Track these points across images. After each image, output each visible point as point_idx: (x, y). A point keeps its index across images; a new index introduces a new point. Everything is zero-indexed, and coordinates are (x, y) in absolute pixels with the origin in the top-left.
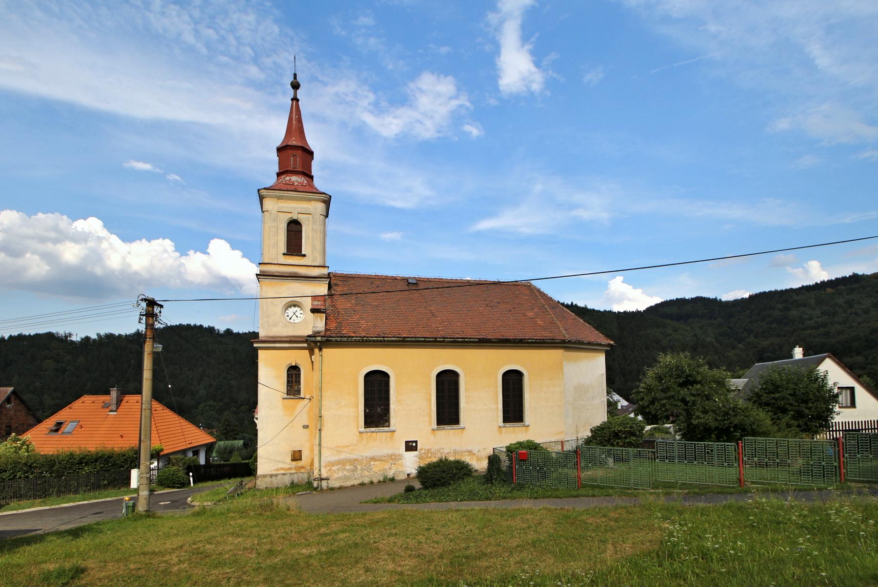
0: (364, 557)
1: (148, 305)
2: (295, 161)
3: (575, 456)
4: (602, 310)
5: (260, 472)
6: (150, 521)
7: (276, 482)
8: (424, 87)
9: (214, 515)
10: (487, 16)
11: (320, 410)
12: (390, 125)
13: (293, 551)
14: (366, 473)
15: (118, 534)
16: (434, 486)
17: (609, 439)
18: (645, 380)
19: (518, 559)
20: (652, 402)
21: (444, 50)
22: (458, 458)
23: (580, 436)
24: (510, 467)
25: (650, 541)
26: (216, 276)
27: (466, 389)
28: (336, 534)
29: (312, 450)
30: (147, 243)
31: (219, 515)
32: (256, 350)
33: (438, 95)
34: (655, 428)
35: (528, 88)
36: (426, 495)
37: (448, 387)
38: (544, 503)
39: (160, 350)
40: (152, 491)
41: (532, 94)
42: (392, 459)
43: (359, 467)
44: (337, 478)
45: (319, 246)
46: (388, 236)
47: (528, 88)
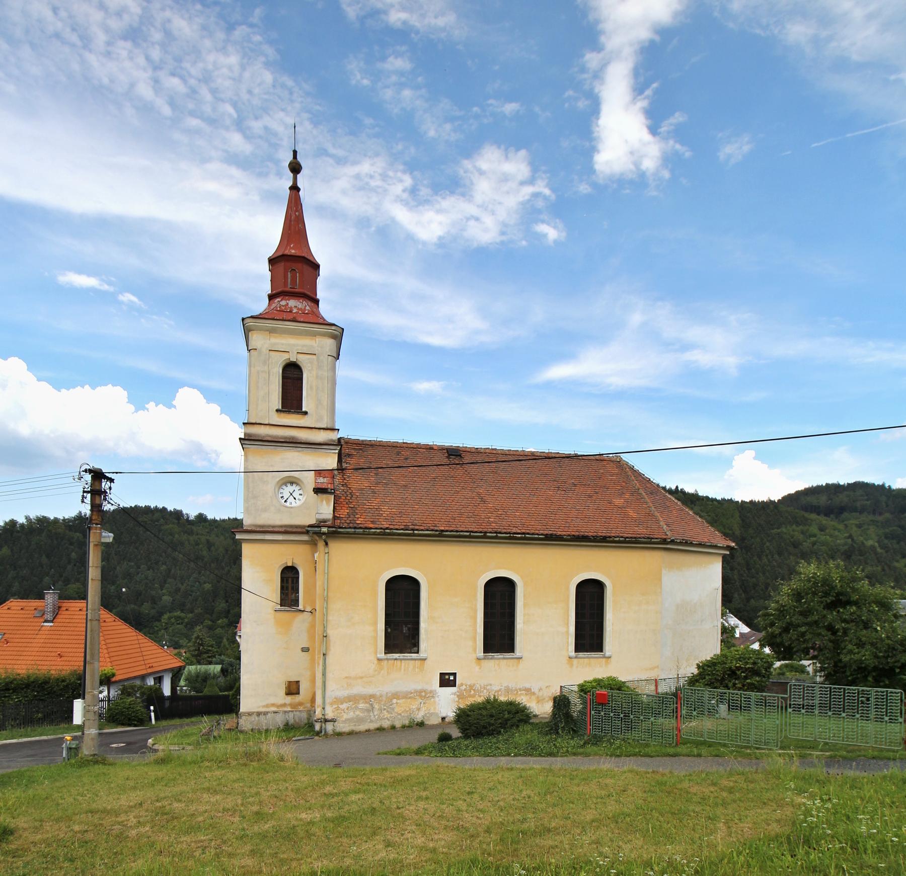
0: (384, 826)
3: (673, 702)
4: (719, 498)
5: (243, 708)
6: (98, 769)
7: (264, 722)
9: (184, 763)
10: (583, 56)
12: (430, 224)
13: (289, 815)
14: (386, 714)
15: (57, 784)
16: (478, 734)
17: (723, 679)
19: (593, 838)
22: (511, 698)
23: (682, 672)
24: (582, 713)
25: (778, 821)
27: (525, 605)
28: (346, 795)
31: (190, 763)
33: (505, 178)
34: (786, 666)
35: (637, 164)
37: (500, 598)
38: (630, 764)
41: (642, 175)
42: (421, 697)
43: (376, 706)
44: (346, 718)
46: (423, 386)
47: (637, 164)
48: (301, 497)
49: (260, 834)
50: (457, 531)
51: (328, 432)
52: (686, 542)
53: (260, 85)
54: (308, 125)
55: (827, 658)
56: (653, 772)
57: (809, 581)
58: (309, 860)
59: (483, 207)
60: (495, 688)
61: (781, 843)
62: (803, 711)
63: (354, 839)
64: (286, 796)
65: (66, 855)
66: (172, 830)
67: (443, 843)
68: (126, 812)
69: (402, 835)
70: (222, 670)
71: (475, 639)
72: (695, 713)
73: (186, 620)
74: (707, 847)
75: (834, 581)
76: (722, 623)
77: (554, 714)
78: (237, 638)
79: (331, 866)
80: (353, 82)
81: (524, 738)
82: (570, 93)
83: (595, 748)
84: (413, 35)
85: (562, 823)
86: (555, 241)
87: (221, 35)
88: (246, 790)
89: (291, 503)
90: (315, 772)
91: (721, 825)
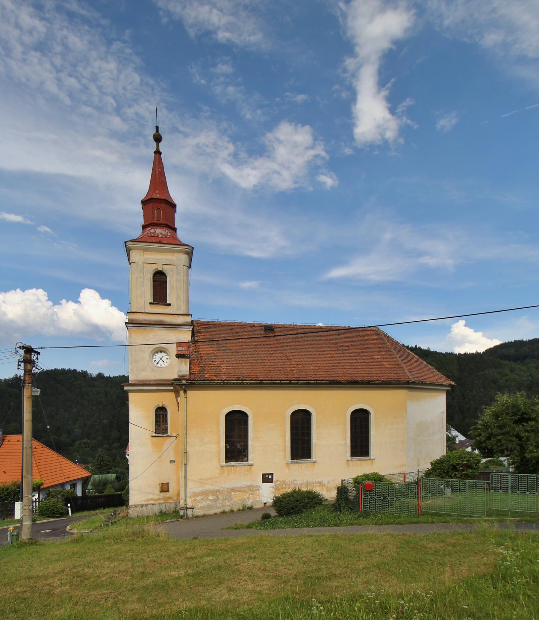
0: (227, 578)
1: (26, 352)
2: (159, 215)
3: (416, 487)
4: (444, 352)
5: (131, 502)
6: (32, 548)
7: (145, 511)
8: (282, 137)
9: (92, 542)
10: (344, 61)
11: (186, 447)
12: (248, 177)
13: (163, 573)
15: (4, 560)
16: (288, 513)
17: (448, 472)
18: (483, 417)
19: (365, 580)
20: (489, 438)
21: (301, 98)
22: (310, 488)
23: (421, 468)
24: (357, 497)
25: (485, 565)
26: (89, 323)
27: (318, 427)
28: (202, 558)
29: (178, 482)
30: (22, 293)
31: (96, 541)
32: (127, 392)
33: (296, 145)
34: (490, 461)
35: (382, 135)
36: (281, 522)
37: (301, 424)
38: (387, 530)
39: (39, 393)
40: (34, 520)
41: (386, 142)
42: (250, 490)
44: (201, 506)
45: (183, 296)
46: (247, 285)
47: (382, 135)
48: (167, 361)
49: (144, 587)
50: (272, 380)
51: (185, 316)
52: (422, 383)
53: (131, 83)
54: (165, 111)
55: (516, 456)
56: (403, 535)
57: (503, 406)
58: (177, 603)
59: (282, 165)
60: (299, 482)
61: (487, 579)
62: (501, 491)
63: (207, 587)
64: (161, 560)
65: (11, 609)
66: (84, 587)
67: (266, 587)
68: (53, 577)
69: (239, 583)
70: (117, 477)
71: (285, 451)
72: (430, 495)
73: (91, 445)
74: (439, 583)
75: (520, 405)
76: (447, 434)
77: (338, 499)
78: (126, 456)
79: (192, 606)
80: (195, 81)
81: (319, 515)
82: (336, 87)
83: (365, 520)
84: (234, 49)
85: (344, 570)
86: (332, 187)
87: (103, 49)
88: (134, 557)
89: (161, 365)
90: (181, 543)
91: (448, 568)
